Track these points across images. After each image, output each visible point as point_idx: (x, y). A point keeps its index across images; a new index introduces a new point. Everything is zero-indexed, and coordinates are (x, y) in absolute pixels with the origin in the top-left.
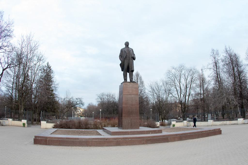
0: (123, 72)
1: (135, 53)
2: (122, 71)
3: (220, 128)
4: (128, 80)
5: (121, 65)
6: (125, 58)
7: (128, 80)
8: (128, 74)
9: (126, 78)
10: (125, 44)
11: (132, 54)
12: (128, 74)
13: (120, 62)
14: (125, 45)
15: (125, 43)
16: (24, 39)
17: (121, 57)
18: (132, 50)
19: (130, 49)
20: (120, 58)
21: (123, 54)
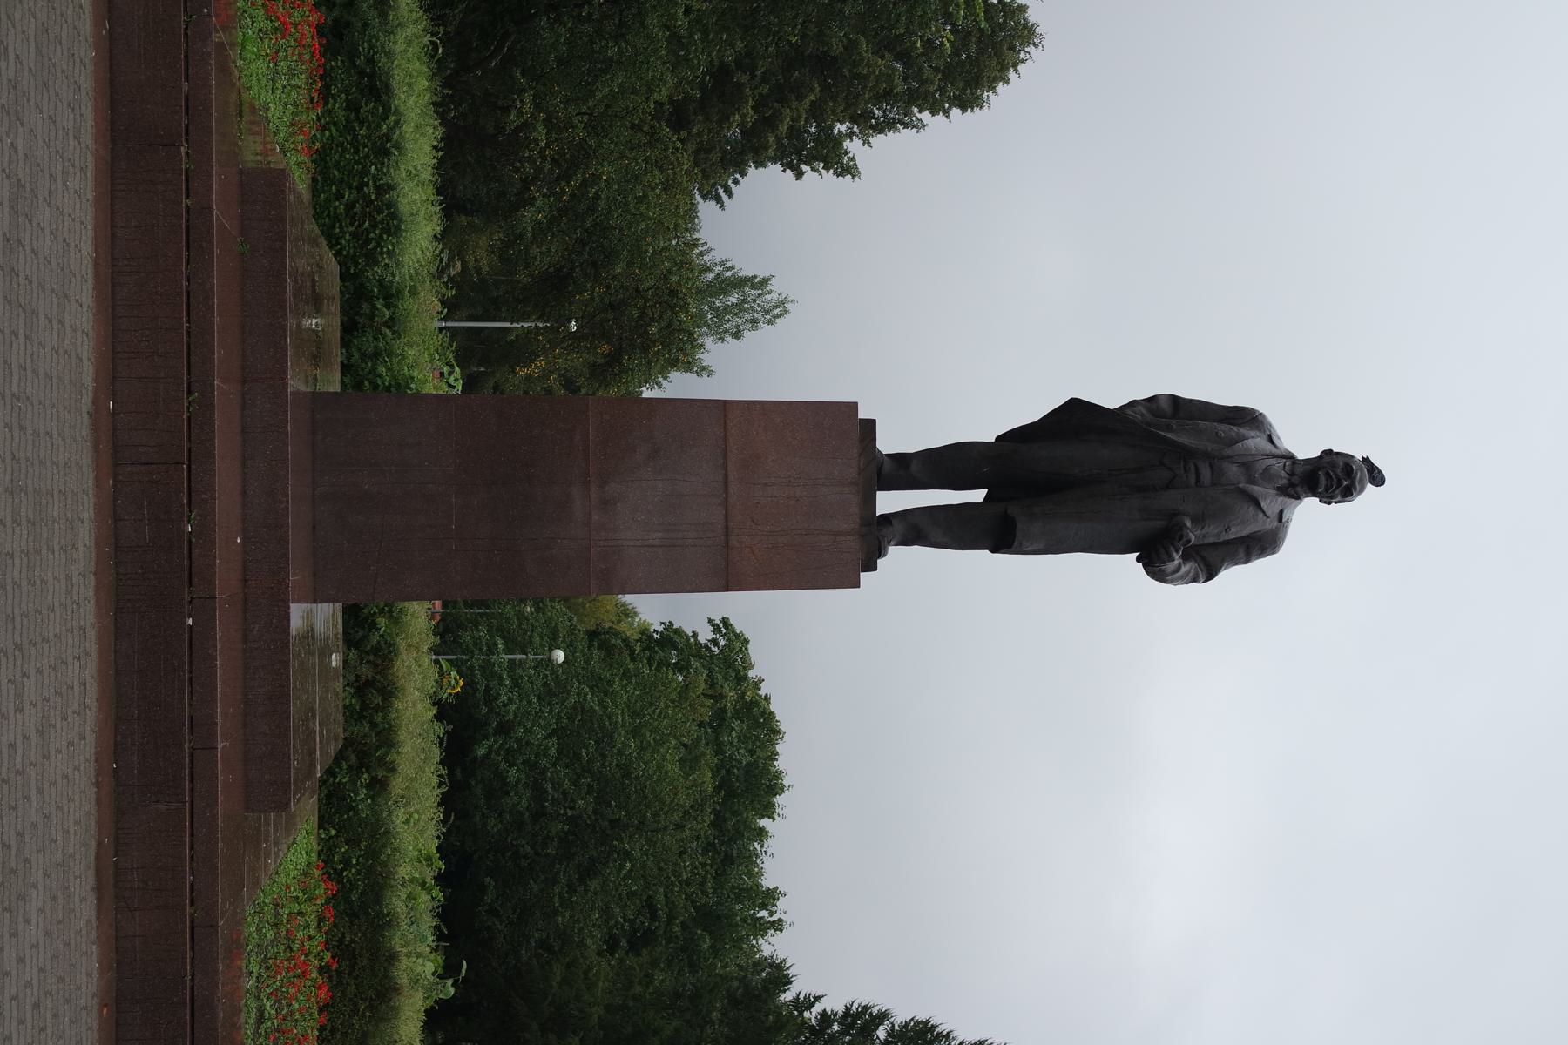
1: (1231, 576)
2: (998, 438)
4: (889, 502)
7: (889, 502)
9: (915, 467)
10: (1328, 453)
11: (1212, 532)
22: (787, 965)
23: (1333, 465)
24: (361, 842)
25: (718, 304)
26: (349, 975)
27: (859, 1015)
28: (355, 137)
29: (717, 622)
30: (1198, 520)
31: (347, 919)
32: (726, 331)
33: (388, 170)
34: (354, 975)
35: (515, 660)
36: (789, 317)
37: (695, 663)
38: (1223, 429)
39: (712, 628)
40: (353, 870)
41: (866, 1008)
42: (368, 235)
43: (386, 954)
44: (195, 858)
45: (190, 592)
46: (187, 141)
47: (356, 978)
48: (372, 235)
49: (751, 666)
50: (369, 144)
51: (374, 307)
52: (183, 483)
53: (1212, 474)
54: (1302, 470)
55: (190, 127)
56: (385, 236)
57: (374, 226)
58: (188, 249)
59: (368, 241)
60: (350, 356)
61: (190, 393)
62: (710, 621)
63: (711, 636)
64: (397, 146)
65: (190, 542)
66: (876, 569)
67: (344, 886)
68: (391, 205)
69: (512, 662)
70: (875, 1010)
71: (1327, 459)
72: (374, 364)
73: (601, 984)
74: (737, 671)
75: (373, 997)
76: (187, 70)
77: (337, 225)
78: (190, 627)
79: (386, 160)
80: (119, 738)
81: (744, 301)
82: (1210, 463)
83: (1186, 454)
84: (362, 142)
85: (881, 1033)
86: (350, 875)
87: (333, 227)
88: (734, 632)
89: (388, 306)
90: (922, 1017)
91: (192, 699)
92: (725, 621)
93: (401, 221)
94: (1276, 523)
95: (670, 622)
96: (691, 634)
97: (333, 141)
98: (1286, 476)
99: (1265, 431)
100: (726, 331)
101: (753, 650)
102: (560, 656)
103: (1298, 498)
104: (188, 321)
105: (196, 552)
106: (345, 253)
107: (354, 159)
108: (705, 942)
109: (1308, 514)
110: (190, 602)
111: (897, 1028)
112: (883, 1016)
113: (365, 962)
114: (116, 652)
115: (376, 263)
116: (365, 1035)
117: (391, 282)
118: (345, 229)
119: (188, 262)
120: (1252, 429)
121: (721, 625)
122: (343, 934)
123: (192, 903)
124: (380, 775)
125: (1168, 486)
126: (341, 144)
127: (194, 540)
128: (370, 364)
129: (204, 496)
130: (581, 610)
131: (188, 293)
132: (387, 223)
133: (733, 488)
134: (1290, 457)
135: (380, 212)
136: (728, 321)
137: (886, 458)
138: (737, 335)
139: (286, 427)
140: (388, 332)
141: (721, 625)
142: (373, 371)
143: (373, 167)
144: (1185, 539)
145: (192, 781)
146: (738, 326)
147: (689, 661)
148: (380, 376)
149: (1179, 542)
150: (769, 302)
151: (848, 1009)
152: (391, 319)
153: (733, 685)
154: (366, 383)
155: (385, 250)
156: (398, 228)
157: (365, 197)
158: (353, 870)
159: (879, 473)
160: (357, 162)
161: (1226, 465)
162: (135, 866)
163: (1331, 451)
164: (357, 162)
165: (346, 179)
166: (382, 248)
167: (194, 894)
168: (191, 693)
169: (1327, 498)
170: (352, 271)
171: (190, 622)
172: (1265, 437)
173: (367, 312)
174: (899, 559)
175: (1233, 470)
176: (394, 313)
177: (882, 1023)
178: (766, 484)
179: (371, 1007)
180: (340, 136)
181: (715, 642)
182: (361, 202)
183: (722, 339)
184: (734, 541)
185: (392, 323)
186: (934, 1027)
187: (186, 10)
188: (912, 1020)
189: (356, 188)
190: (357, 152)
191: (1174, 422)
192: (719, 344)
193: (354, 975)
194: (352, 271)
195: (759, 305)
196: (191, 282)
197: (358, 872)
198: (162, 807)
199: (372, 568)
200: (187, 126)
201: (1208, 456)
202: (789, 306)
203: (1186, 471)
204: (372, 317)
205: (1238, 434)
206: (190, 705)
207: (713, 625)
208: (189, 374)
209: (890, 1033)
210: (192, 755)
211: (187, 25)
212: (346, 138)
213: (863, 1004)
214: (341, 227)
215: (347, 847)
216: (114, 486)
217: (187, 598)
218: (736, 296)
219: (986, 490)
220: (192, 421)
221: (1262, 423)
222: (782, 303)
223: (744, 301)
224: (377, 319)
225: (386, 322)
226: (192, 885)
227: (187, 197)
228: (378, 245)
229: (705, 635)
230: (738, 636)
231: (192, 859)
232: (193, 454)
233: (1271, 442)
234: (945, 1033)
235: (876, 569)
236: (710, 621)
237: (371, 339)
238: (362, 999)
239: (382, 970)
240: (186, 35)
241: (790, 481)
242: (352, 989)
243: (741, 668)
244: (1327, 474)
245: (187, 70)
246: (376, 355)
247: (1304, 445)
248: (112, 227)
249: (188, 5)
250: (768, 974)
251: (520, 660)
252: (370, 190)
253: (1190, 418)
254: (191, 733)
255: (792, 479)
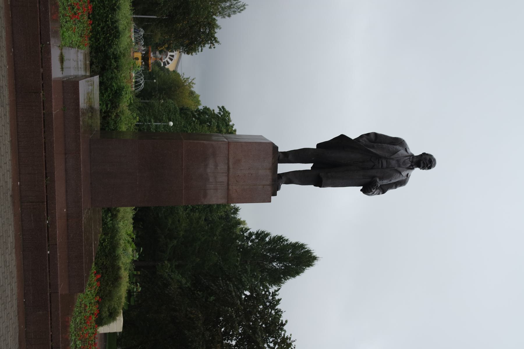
0: (315, 147)
1: (390, 192)
2: (318, 145)
3: (173, 55)
4: (283, 168)
5: (342, 138)
6: (370, 152)
7: (283, 168)
8: (308, 166)
9: (290, 157)
10: (424, 154)
11: (385, 182)
12: (308, 166)
13: (353, 135)
14: (421, 155)
15: (431, 156)
16: (2, 306)
17: (373, 137)
18: (402, 183)
19: (404, 174)
20: (368, 134)
21: (385, 145)
22: (239, 209)
23: (425, 159)
24: (109, 234)
25: (223, 6)
26: (106, 273)
27: (261, 234)
28: (104, 4)
29: (220, 107)
30: (381, 179)
31: (104, 257)
32: (225, 14)
33: (115, 16)
34: (107, 273)
35: (158, 125)
36: (245, 10)
37: (213, 121)
38: (391, 147)
39: (219, 109)
40: (106, 243)
41: (263, 232)
42: (108, 38)
43: (117, 267)
44: (52, 327)
45: (48, 243)
46: (43, 90)
47: (108, 274)
48: (110, 38)
49: (231, 121)
50: (109, 6)
51: (111, 62)
52: (45, 209)
53: (387, 164)
54: (415, 160)
55: (44, 85)
56: (114, 39)
57: (111, 35)
58: (44, 128)
59: (109, 40)
60: (103, 79)
61: (46, 177)
62: (218, 107)
63: (218, 111)
64: (119, 7)
65: (48, 227)
66: (276, 195)
67: (103, 247)
68: (116, 28)
69: (156, 125)
70: (266, 233)
71: (424, 157)
72: (111, 82)
73: (183, 225)
74: (226, 123)
75: (113, 280)
76: (42, 64)
77: (98, 35)
78: (49, 254)
79: (114, 13)
80: (25, 291)
81: (231, 5)
82: (386, 160)
83: (379, 157)
84: (106, 6)
85: (267, 239)
86: (105, 244)
87: (97, 35)
88: (226, 110)
89: (115, 61)
90: (280, 235)
91: (50, 277)
92: (223, 107)
93: (120, 33)
94: (406, 177)
95: (206, 106)
96: (212, 110)
97: (96, 6)
98: (410, 163)
99: (404, 147)
100: (225, 14)
101: (231, 116)
102: (171, 124)
103: (413, 169)
104: (45, 152)
105: (50, 230)
106: (101, 44)
107: (104, 12)
108: (215, 206)
109: (417, 173)
110: (49, 246)
111: (272, 238)
112: (268, 235)
113: (110, 270)
114: (23, 264)
115: (112, 47)
116: (110, 291)
117: (117, 54)
118: (101, 36)
119: (44, 132)
120: (400, 146)
121: (222, 108)
122: (103, 262)
123: (52, 341)
124: (115, 213)
125: (372, 168)
126: (99, 7)
127: (49, 226)
128: (110, 82)
129: (52, 211)
130: (178, 95)
131: (45, 143)
132: (115, 34)
133: (231, 170)
134: (412, 155)
135: (113, 30)
136: (226, 11)
137: (280, 153)
138: (229, 16)
139: (81, 169)
140: (116, 71)
141: (222, 108)
142: (111, 84)
143: (110, 15)
144: (376, 186)
145: (50, 302)
146: (229, 13)
147: (211, 120)
148: (113, 86)
149: (375, 186)
150: (239, 5)
151: (257, 232)
152: (117, 66)
153: (225, 127)
154: (109, 89)
155: (114, 43)
156: (119, 36)
157: (108, 25)
158: (106, 243)
159: (278, 159)
160: (105, 13)
161: (391, 161)
162: (32, 331)
163: (425, 153)
164: (105, 13)
165: (101, 18)
166: (114, 43)
167: (52, 338)
168: (49, 275)
169: (423, 168)
170: (103, 50)
171: (49, 252)
172: (404, 149)
173: (109, 64)
174: (284, 188)
175: (393, 163)
176: (118, 64)
177: (267, 236)
178: (241, 169)
179: (113, 284)
180: (99, 4)
181: (220, 113)
182: (106, 27)
183: (224, 17)
184: (230, 187)
185: (117, 68)
186: (283, 238)
187: (41, 43)
188: (277, 236)
189: (105, 22)
190: (105, 9)
191: (375, 145)
192: (223, 19)
193: (107, 273)
194: (103, 50)
195: (236, 6)
196: (46, 139)
197: (108, 243)
198: (41, 313)
199: (111, 196)
200: (43, 84)
201: (386, 158)
202: (246, 7)
203: (378, 163)
204: (110, 66)
205: (396, 149)
206: (49, 279)
207: (219, 108)
208: (46, 170)
209: (270, 239)
210: (50, 295)
211: (41, 48)
212: (101, 5)
213: (262, 231)
214: (100, 36)
215: (104, 236)
216: (21, 210)
217: (47, 245)
218: (229, 3)
219: (313, 164)
220: (47, 186)
221: (404, 144)
222: (244, 5)
223: (231, 5)
224: (112, 67)
225: (115, 67)
226: (51, 335)
227: (44, 110)
228: (112, 42)
229: (217, 111)
230: (227, 112)
231: (51, 327)
232: (48, 197)
233: (406, 151)
234: (286, 239)
235: (276, 195)
236: (218, 107)
237: (110, 73)
238: (109, 281)
239: (116, 272)
240: (41, 52)
241: (249, 168)
242: (106, 278)
243: (227, 122)
244: (424, 162)
245: (42, 64)
246: (112, 78)
247: (415, 150)
248: (17, 122)
249: (42, 40)
250: (233, 211)
251: (159, 125)
252: (109, 23)
253: (380, 143)
254: (50, 288)
255: (250, 168)
